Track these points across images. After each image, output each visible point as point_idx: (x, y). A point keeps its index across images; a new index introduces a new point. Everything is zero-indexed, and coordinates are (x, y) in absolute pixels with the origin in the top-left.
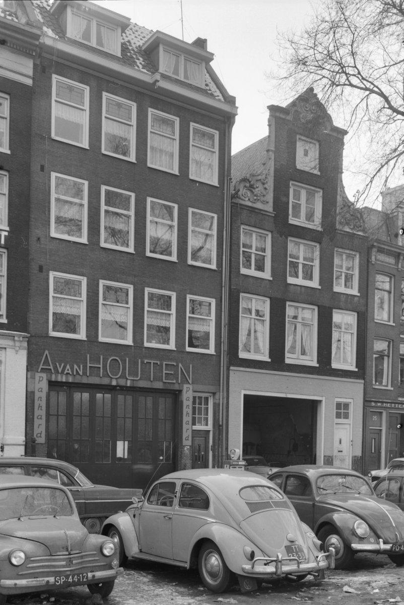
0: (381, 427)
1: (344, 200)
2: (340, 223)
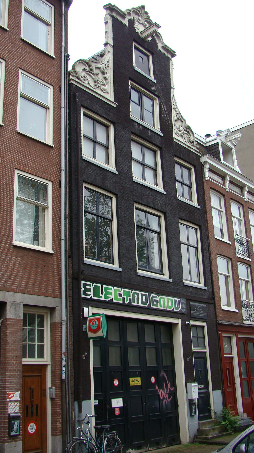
0: (231, 354)
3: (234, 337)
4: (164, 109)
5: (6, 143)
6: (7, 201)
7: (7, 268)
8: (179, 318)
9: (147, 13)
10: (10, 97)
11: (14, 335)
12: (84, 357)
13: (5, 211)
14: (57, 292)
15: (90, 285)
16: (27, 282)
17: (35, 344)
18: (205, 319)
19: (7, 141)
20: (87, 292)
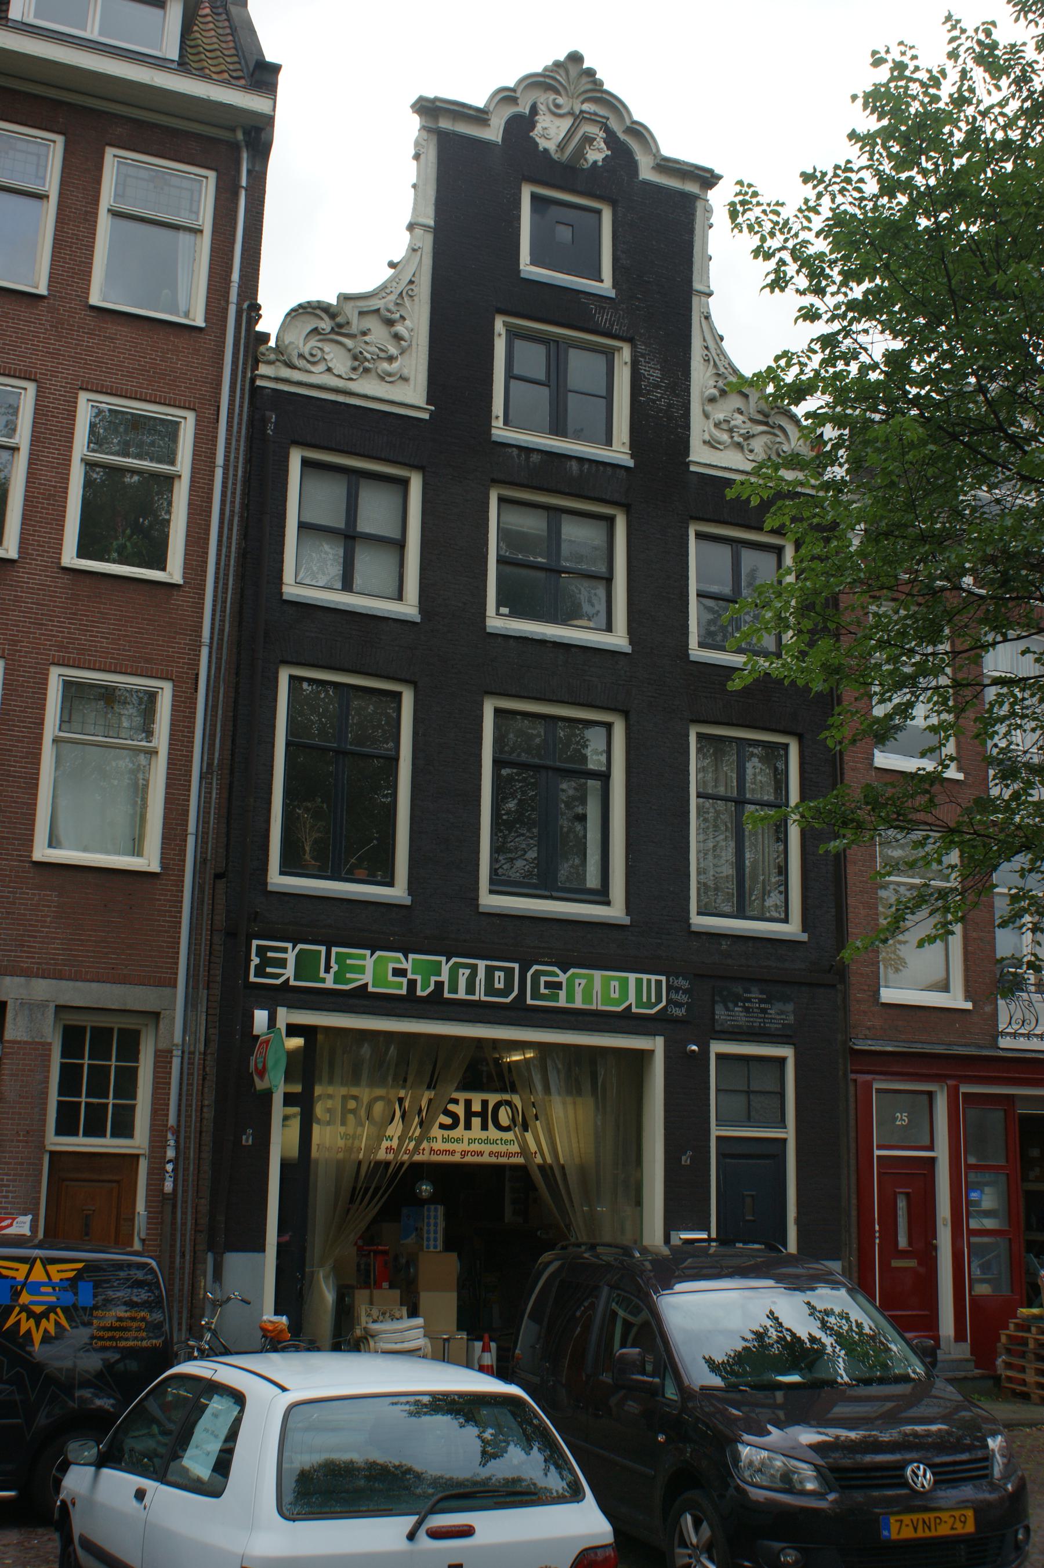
0: (931, 1148)
1: (718, 375)
2: (711, 444)
3: (942, 1090)
4: (653, 373)
5: (27, 603)
6: (22, 752)
7: (12, 919)
8: (655, 1035)
9: (591, 73)
10: (46, 476)
11: (22, 1081)
12: (247, 1141)
13: (14, 777)
14: (167, 973)
15: (284, 950)
16: (71, 950)
17: (108, 1104)
18: (790, 1036)
19: (26, 597)
20: (269, 970)
